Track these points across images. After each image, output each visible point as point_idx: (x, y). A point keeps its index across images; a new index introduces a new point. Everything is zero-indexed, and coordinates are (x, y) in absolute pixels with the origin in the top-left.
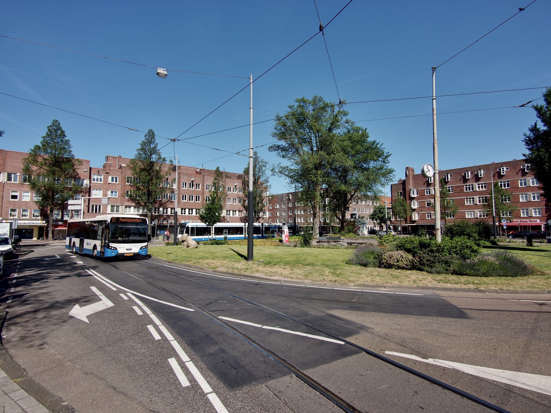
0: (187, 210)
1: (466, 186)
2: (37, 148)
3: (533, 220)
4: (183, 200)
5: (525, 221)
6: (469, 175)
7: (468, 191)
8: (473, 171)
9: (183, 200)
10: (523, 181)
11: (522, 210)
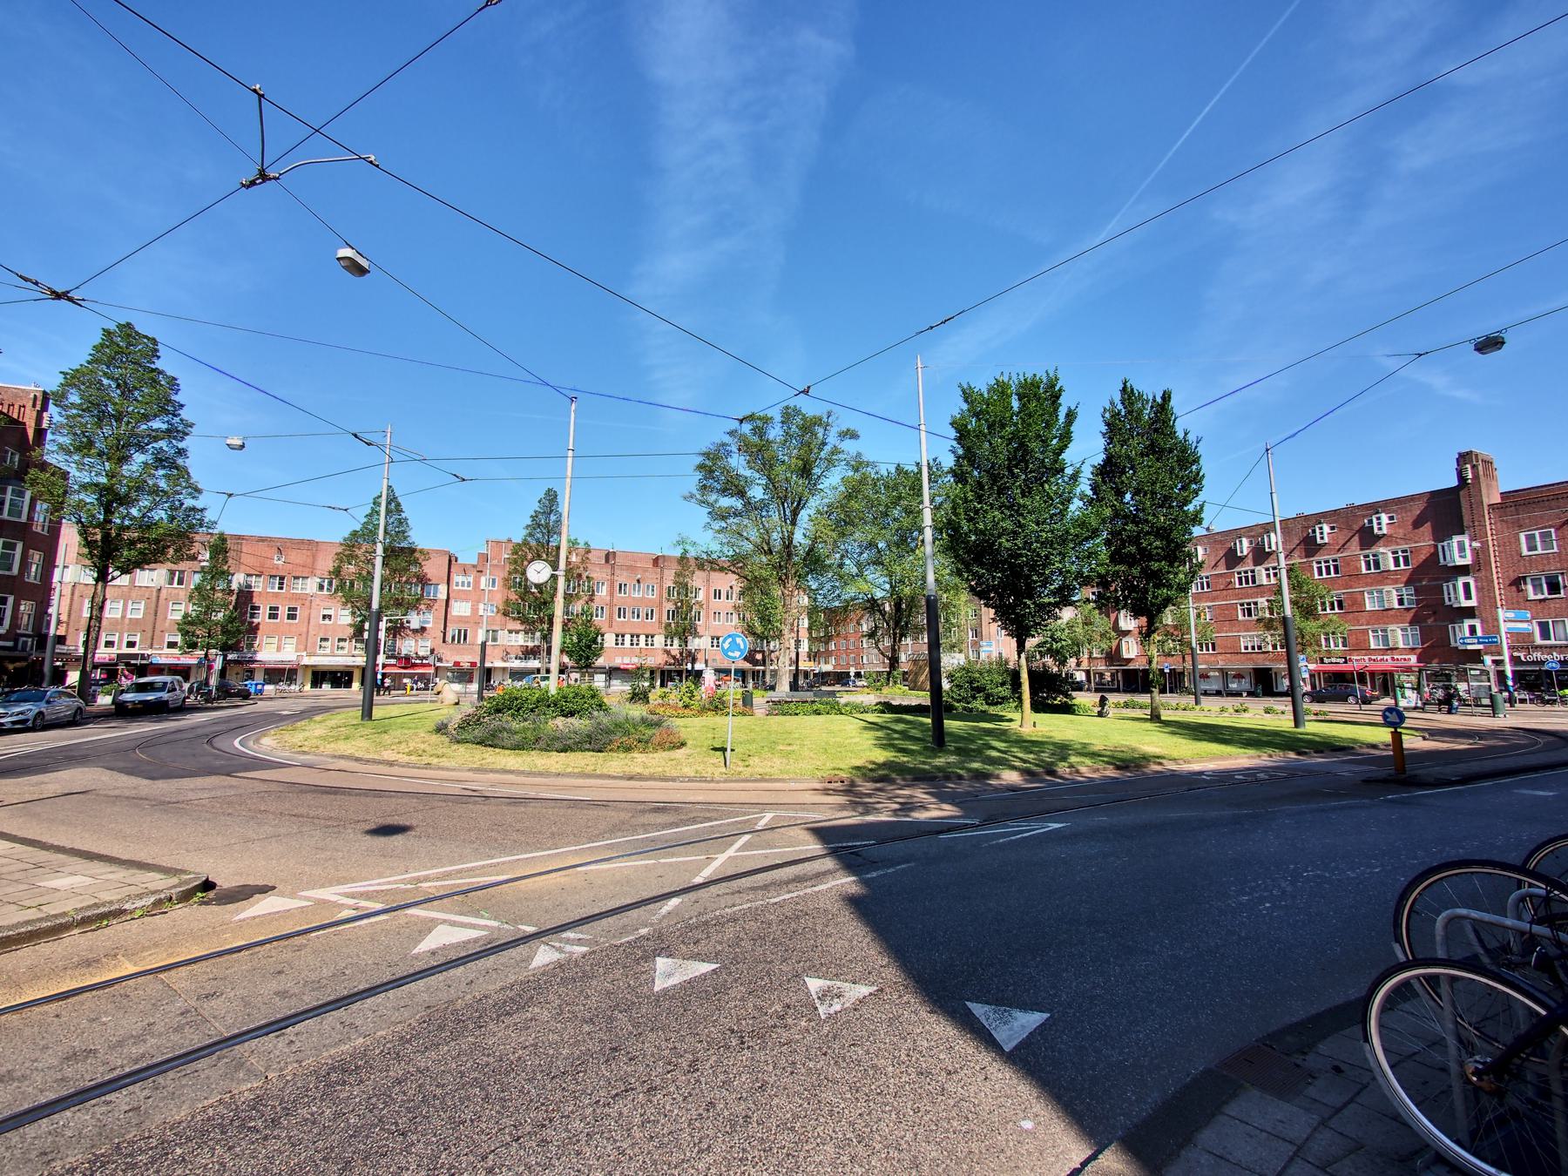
0: (642, 638)
1: (1239, 573)
2: (355, 533)
3: (1399, 657)
4: (619, 617)
5: (1381, 660)
6: (1245, 546)
7: (1244, 585)
8: (1253, 537)
9: (619, 617)
10: (1400, 553)
11: (1373, 631)
